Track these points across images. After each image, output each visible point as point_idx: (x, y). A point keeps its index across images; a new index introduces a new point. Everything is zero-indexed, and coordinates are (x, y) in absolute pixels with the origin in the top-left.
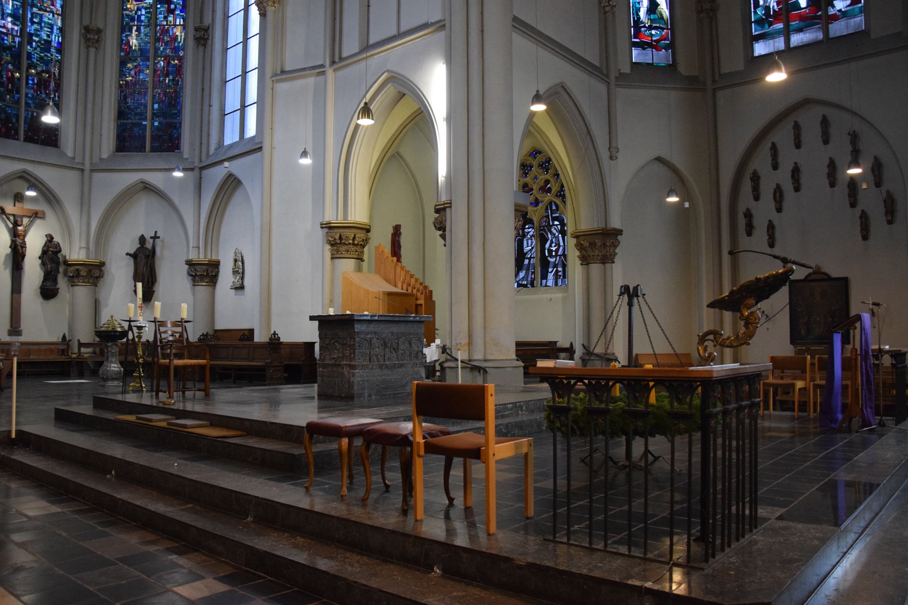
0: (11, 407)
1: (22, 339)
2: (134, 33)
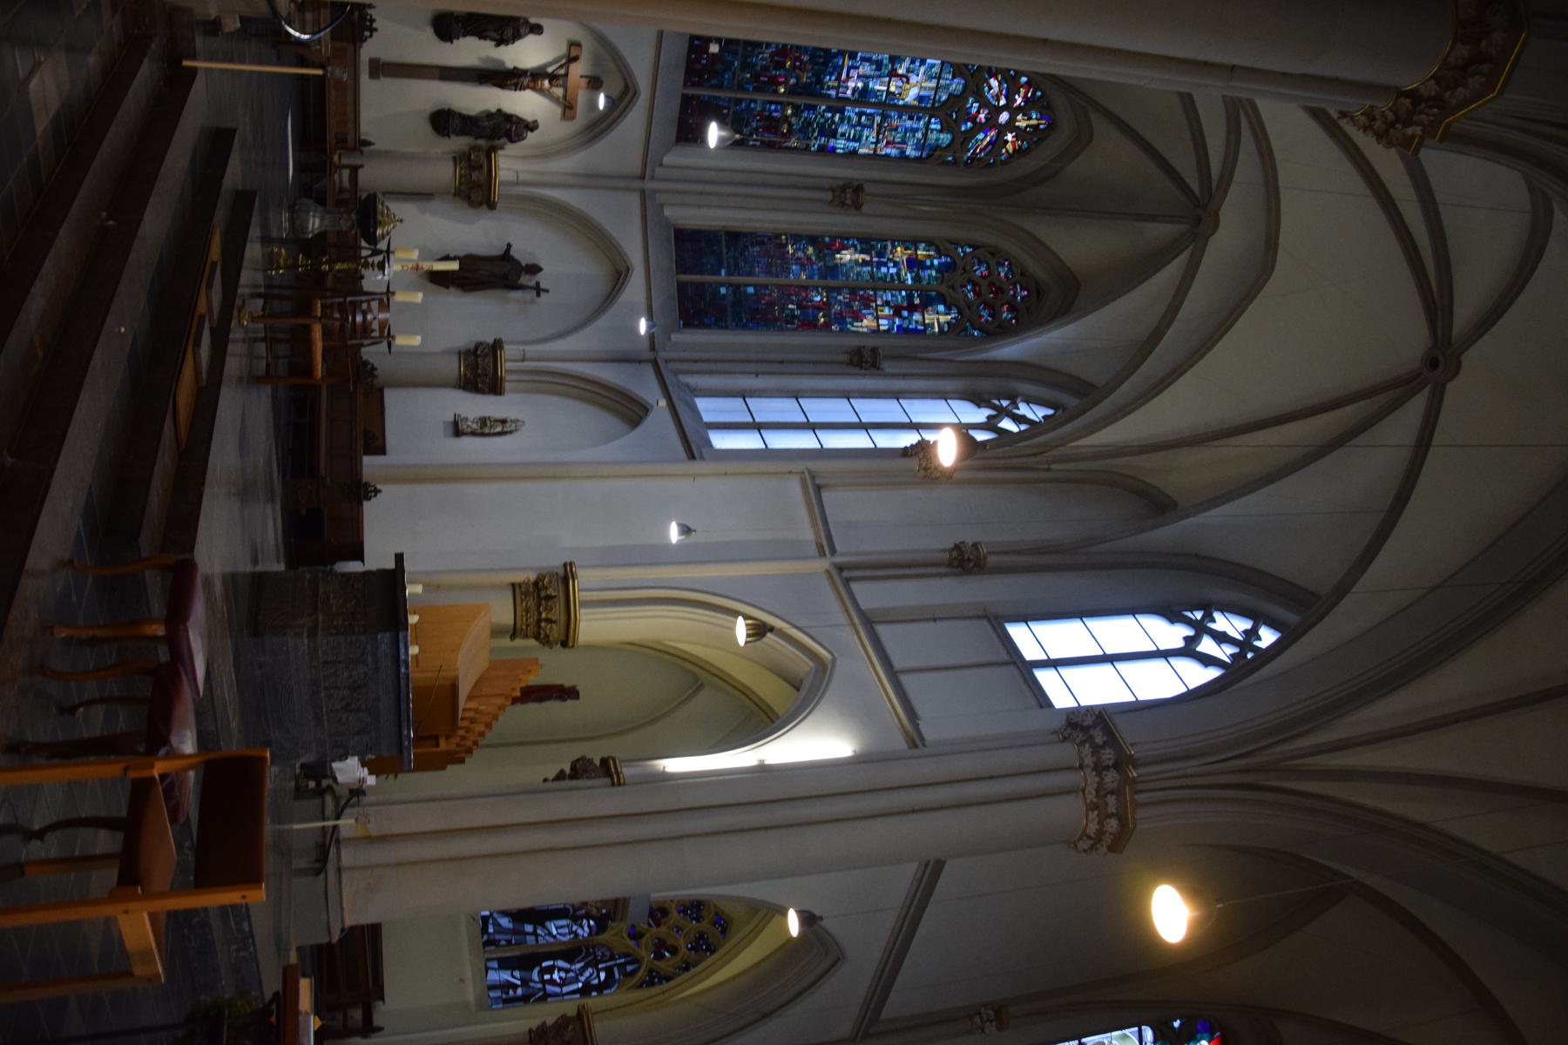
0: (242, 62)
1: (364, 78)
2: (860, 257)
